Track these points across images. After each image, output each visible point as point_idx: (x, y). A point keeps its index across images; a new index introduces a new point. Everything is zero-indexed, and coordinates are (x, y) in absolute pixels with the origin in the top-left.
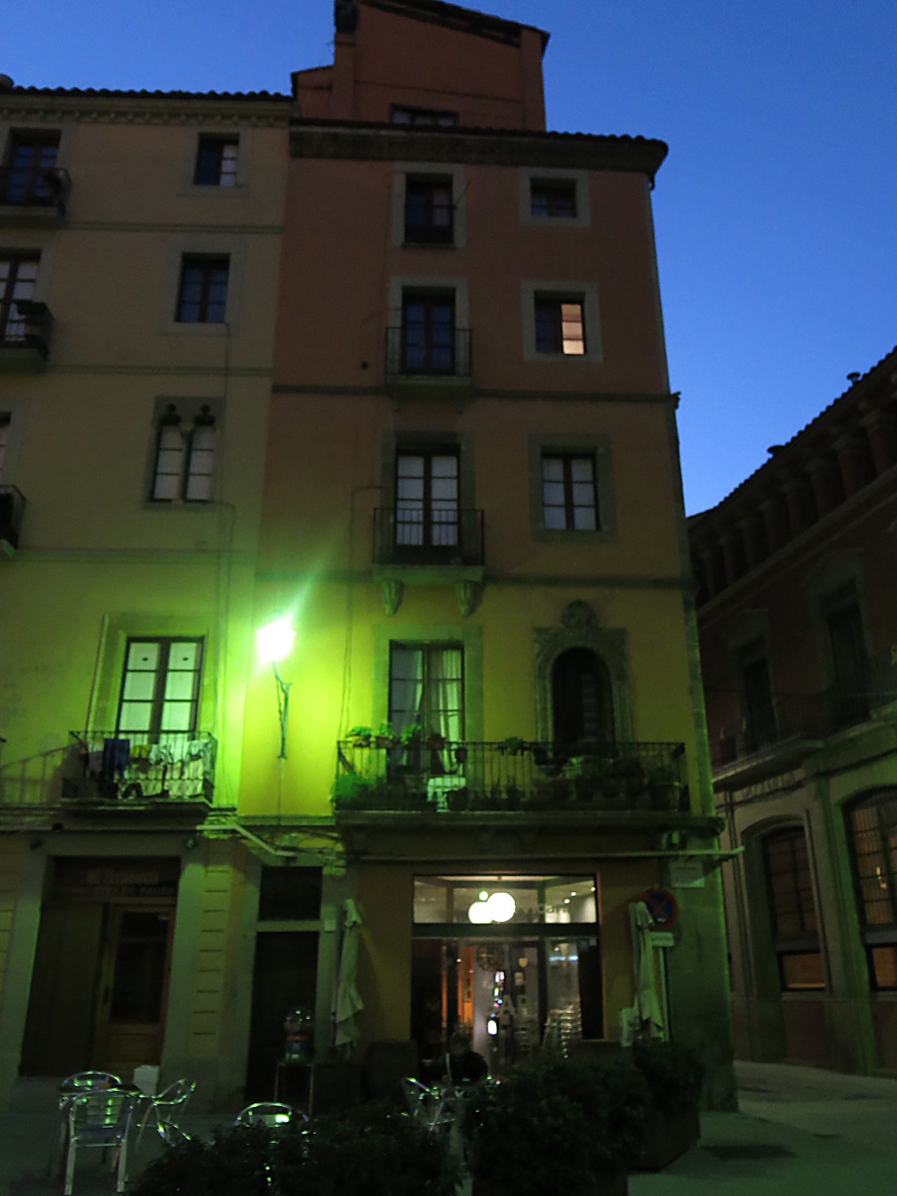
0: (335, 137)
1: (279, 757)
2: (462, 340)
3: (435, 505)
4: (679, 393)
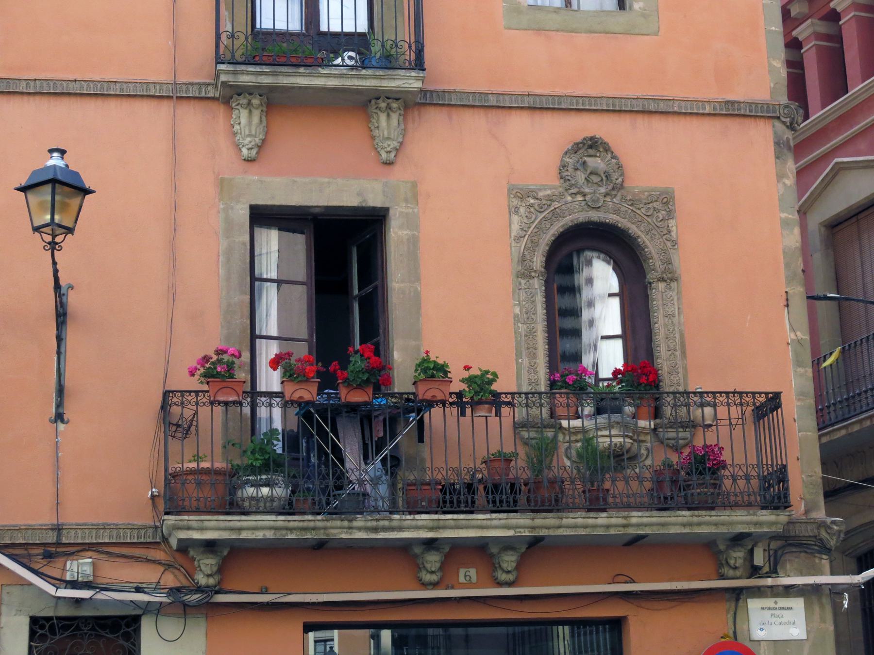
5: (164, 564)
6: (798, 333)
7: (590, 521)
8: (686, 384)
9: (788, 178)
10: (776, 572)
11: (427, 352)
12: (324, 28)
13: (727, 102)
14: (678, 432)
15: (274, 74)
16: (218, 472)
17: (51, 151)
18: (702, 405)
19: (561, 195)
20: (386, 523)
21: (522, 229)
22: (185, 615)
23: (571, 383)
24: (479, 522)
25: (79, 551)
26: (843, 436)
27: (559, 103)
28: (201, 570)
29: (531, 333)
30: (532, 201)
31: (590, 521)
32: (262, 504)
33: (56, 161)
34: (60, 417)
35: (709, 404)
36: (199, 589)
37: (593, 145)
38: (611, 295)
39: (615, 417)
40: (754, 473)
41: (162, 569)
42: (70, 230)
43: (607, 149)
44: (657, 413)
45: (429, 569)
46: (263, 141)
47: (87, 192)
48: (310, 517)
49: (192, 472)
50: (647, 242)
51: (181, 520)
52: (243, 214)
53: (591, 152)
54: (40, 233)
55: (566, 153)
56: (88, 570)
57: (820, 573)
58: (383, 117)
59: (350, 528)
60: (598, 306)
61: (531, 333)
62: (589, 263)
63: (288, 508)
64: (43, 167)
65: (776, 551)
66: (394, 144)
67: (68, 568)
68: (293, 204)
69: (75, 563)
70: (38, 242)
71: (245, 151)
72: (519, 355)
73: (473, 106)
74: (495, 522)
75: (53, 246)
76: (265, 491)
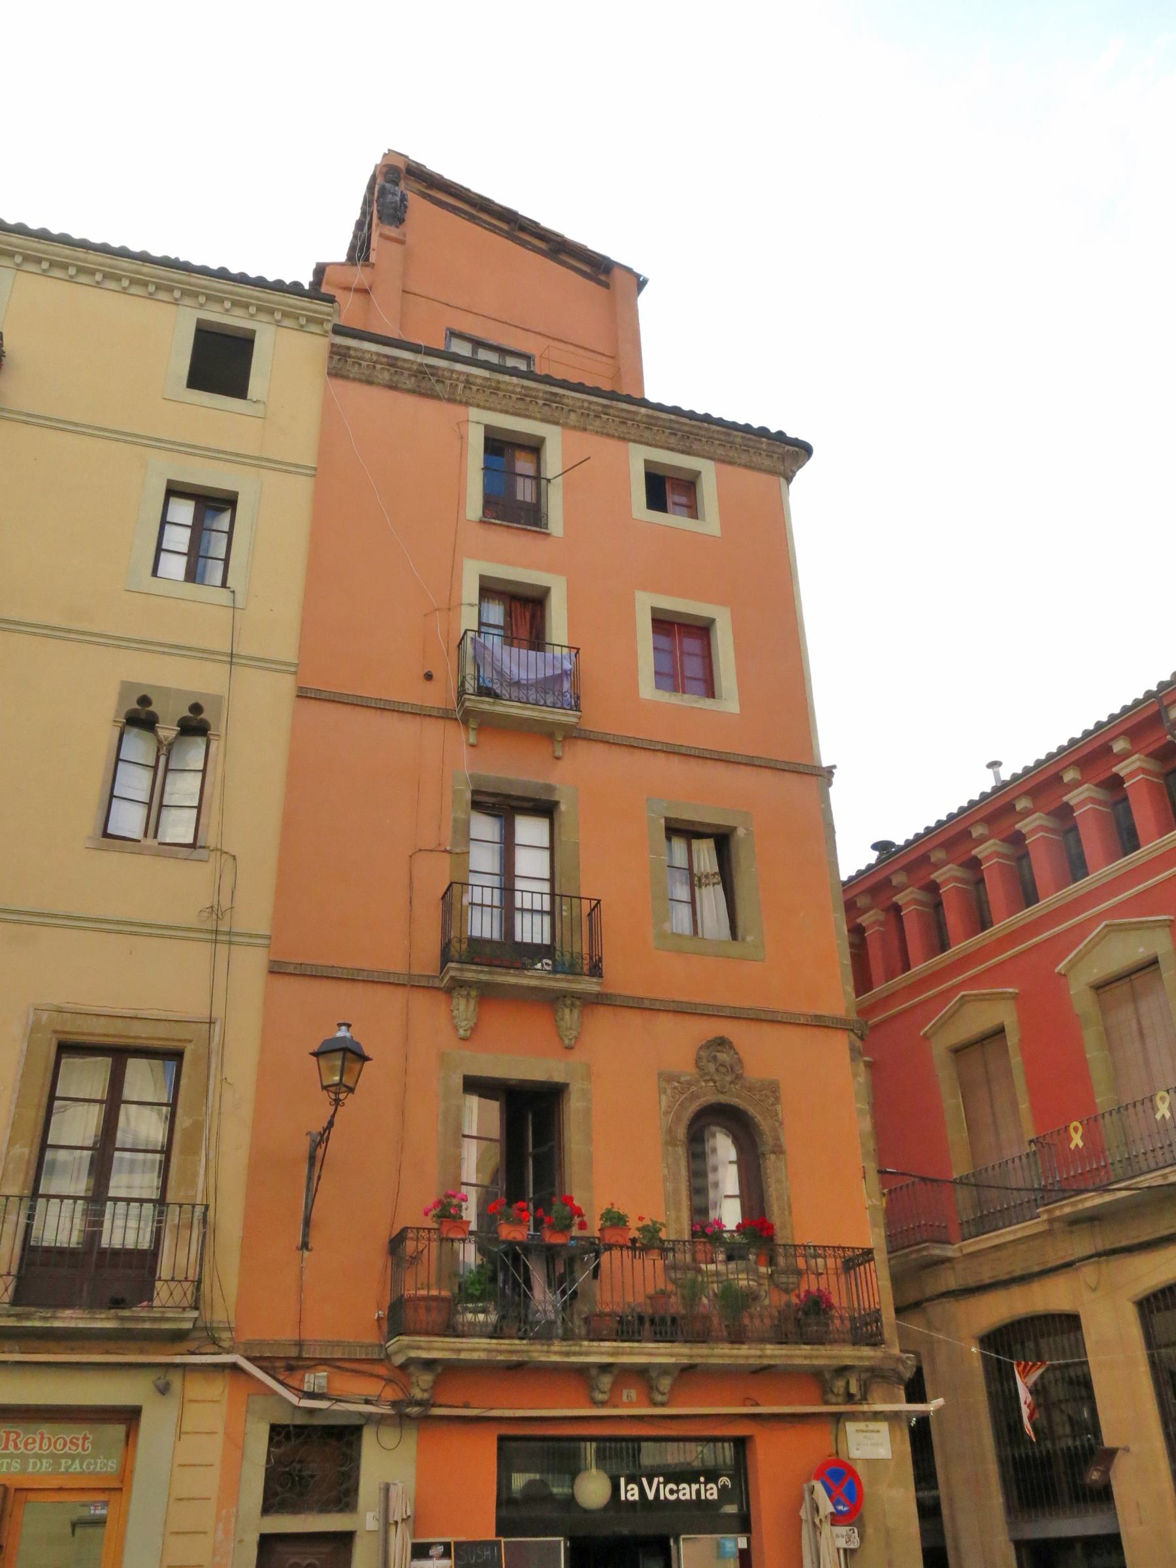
0: (393, 362)
3: (519, 884)
4: (834, 767)
5: (385, 1379)
6: (873, 1200)
7: (735, 1352)
10: (866, 1399)
11: (612, 1204)
12: (518, 938)
14: (788, 1278)
15: (490, 973)
16: (443, 1299)
17: (340, 1025)
18: (815, 1257)
19: (698, 1081)
20: (576, 1349)
21: (669, 1107)
22: (401, 1425)
23: (709, 1234)
24: (650, 1350)
25: (317, 1365)
27: (696, 1009)
28: (418, 1385)
29: (676, 1191)
30: (676, 1084)
31: (735, 1352)
32: (478, 1328)
33: (342, 1033)
34: (305, 1245)
35: (820, 1256)
36: (418, 1403)
37: (721, 1043)
38: (731, 1162)
39: (742, 1264)
41: (383, 1383)
42: (351, 1090)
43: (731, 1046)
44: (772, 1261)
45: (602, 1389)
46: (476, 1024)
47: (366, 1059)
48: (517, 1342)
49: (423, 1298)
51: (414, 1341)
52: (459, 1082)
53: (719, 1048)
54: (328, 1091)
55: (701, 1048)
56: (324, 1382)
57: (897, 1401)
58: (567, 1011)
59: (548, 1352)
60: (721, 1171)
61: (676, 1191)
62: (714, 1136)
63: (496, 1333)
64: (330, 1037)
66: (574, 1033)
67: (306, 1380)
68: (497, 1076)
69: (312, 1376)
70: (325, 1098)
71: (462, 1032)
72: (667, 1209)
73: (632, 1007)
74: (662, 1351)
75: (337, 1102)
76: (481, 1317)
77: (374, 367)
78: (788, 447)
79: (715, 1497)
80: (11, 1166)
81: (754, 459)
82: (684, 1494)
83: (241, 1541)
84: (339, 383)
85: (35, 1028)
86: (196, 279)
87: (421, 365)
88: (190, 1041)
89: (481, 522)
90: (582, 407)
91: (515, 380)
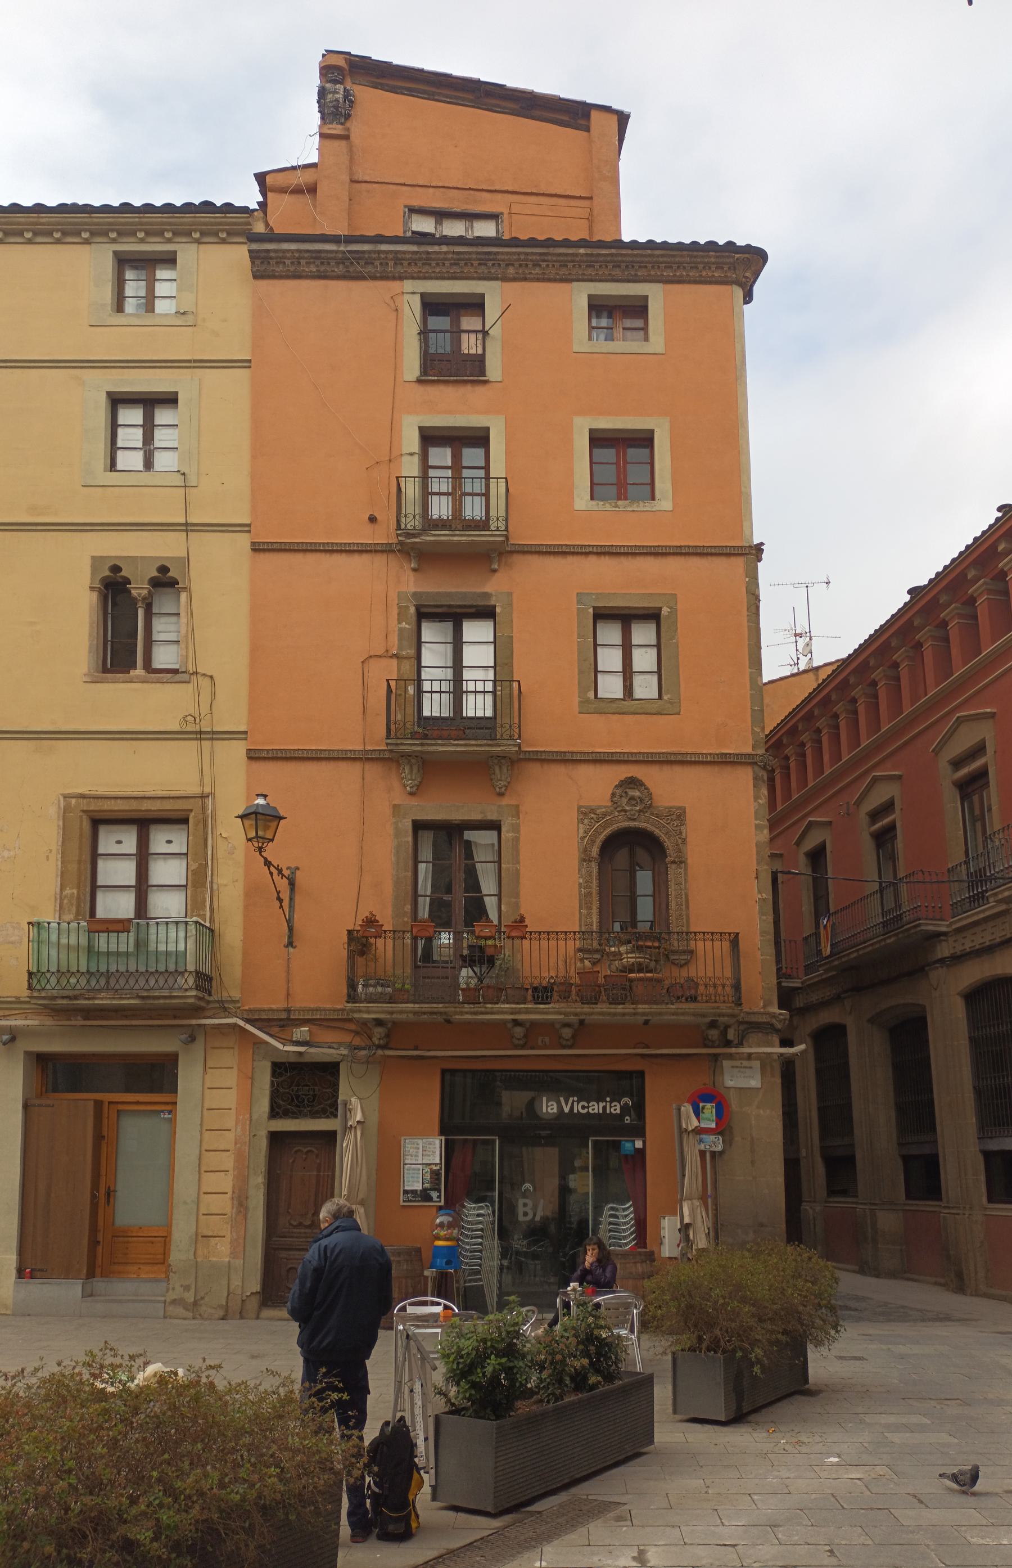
1: (287, 947)
2: (498, 489)
3: (467, 674)
4: (762, 544)
6: (764, 895)
8: (688, 926)
9: (761, 799)
12: (464, 715)
13: (722, 754)
17: (258, 795)
20: (483, 1010)
26: (855, 958)
33: (261, 801)
37: (632, 782)
40: (728, 983)
43: (642, 784)
46: (420, 782)
47: (281, 818)
50: (666, 840)
53: (631, 786)
57: (773, 1046)
65: (743, 1031)
71: (408, 788)
72: (581, 908)
77: (299, 263)
78: (737, 256)
79: (618, 1111)
80: (65, 901)
81: (704, 273)
82: (593, 1110)
83: (255, 1135)
84: (264, 284)
85: (67, 809)
86: (98, 218)
87: (344, 252)
88: (191, 810)
89: (419, 381)
90: (518, 260)
91: (444, 248)
